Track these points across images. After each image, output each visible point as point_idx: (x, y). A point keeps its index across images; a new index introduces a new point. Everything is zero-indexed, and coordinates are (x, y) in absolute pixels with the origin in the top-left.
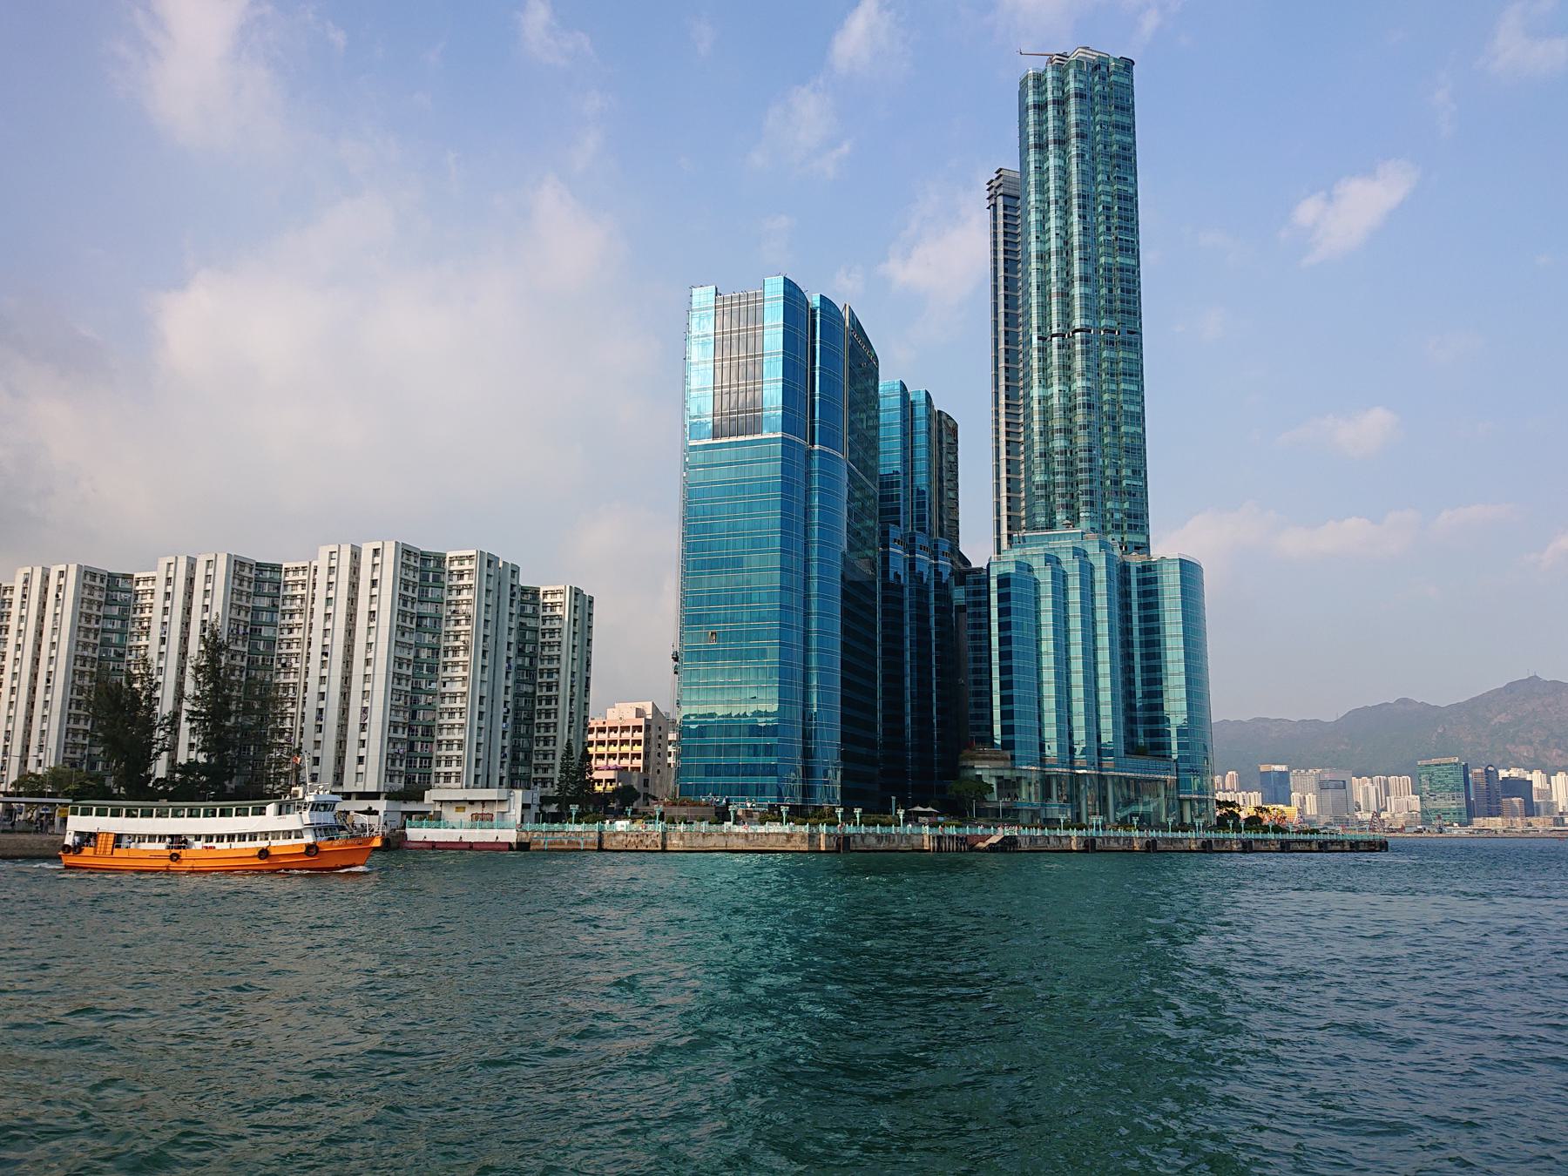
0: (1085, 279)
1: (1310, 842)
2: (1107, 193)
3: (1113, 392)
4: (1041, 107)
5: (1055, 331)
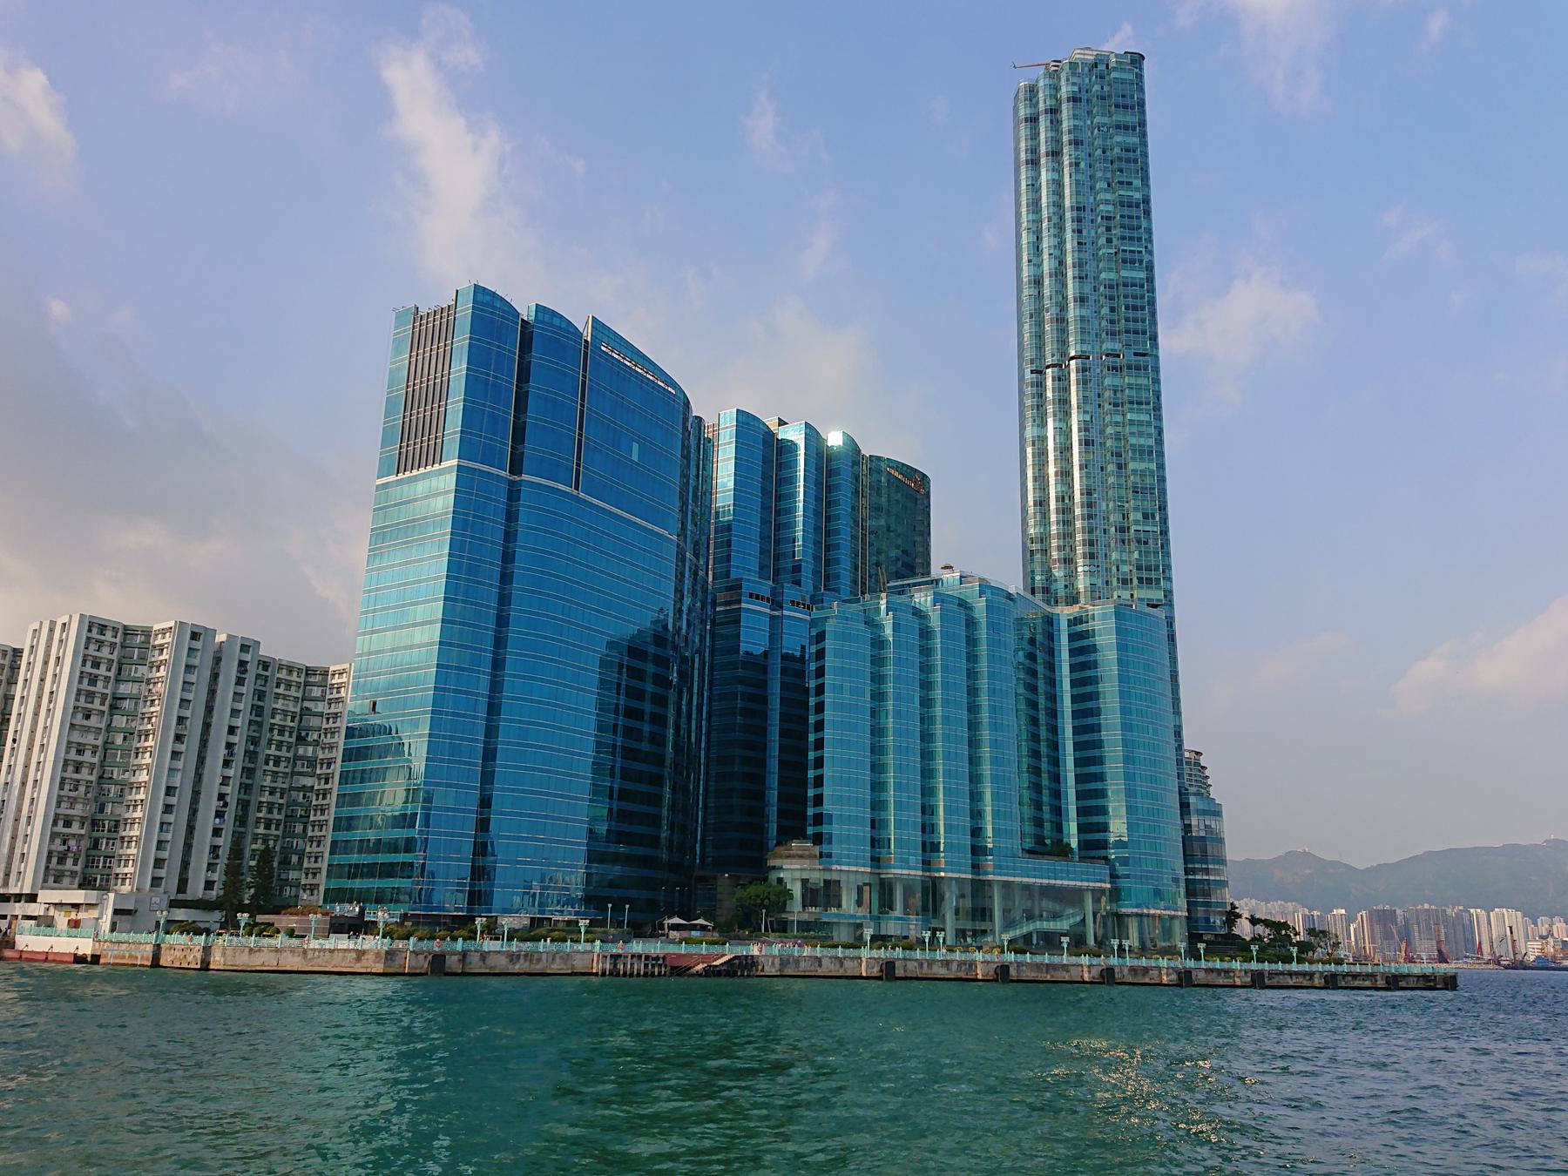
0: (1081, 300)
1: (1311, 975)
2: (1107, 202)
3: (1117, 424)
4: (1033, 120)
5: (1049, 361)
